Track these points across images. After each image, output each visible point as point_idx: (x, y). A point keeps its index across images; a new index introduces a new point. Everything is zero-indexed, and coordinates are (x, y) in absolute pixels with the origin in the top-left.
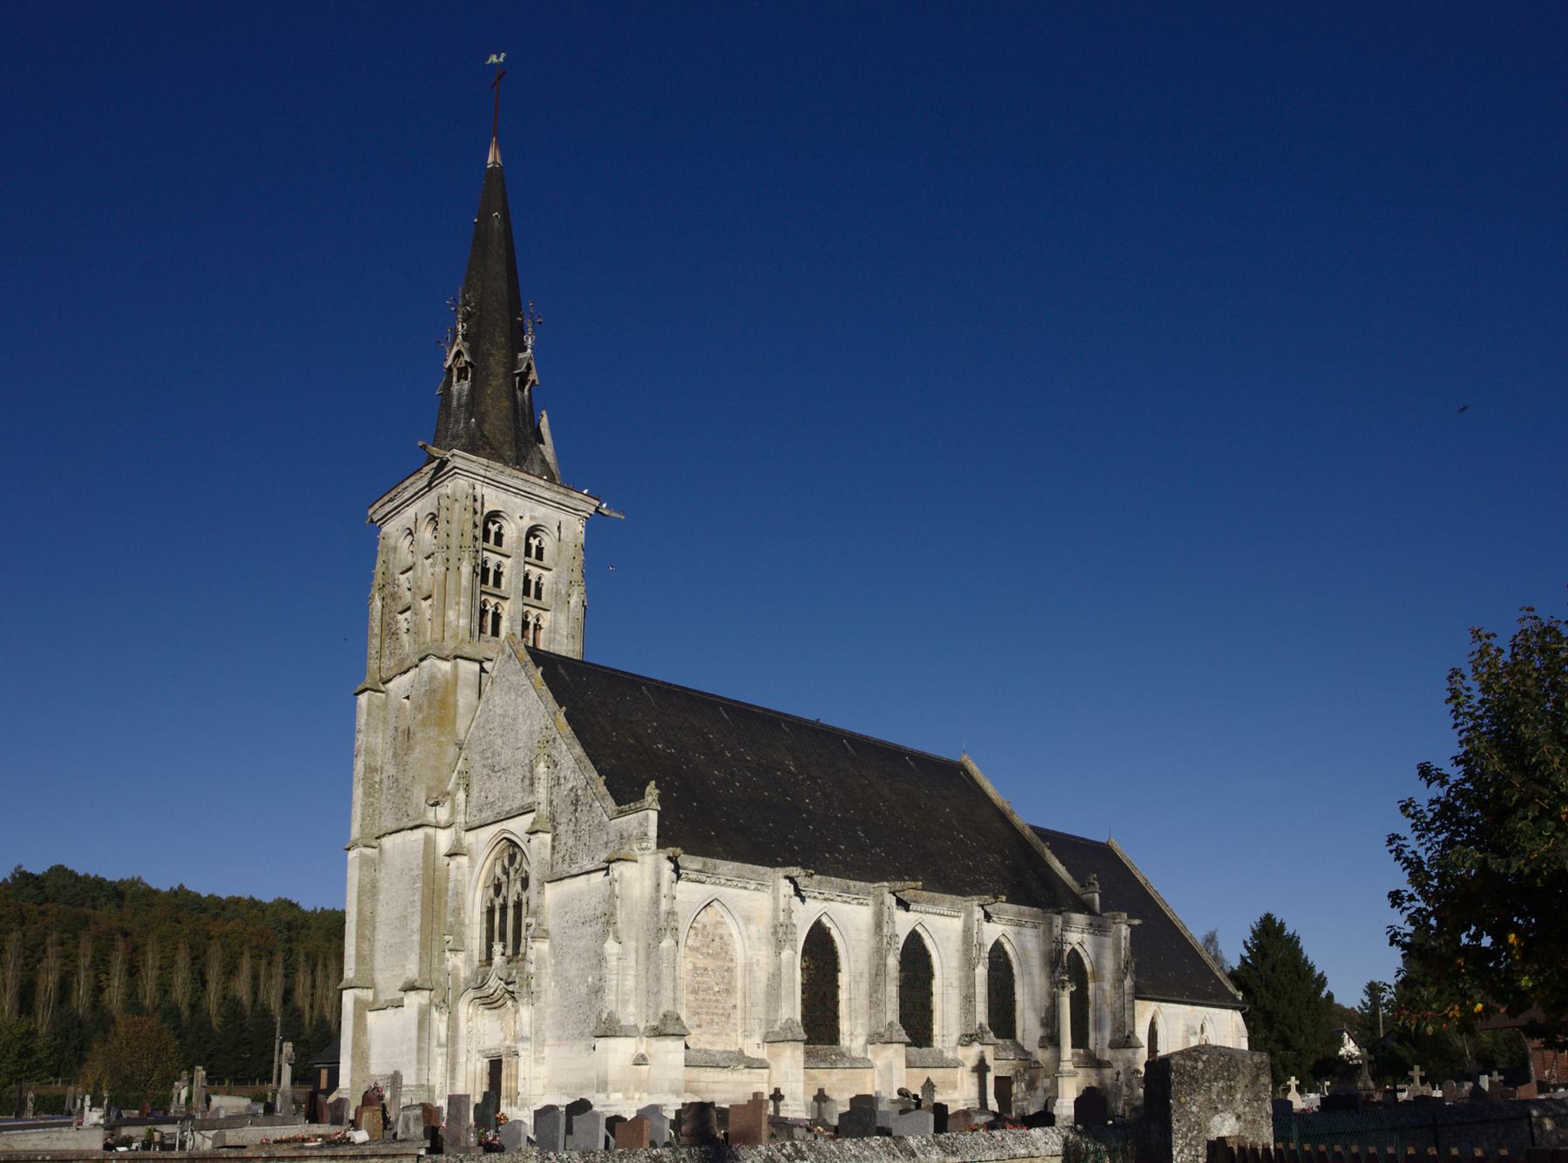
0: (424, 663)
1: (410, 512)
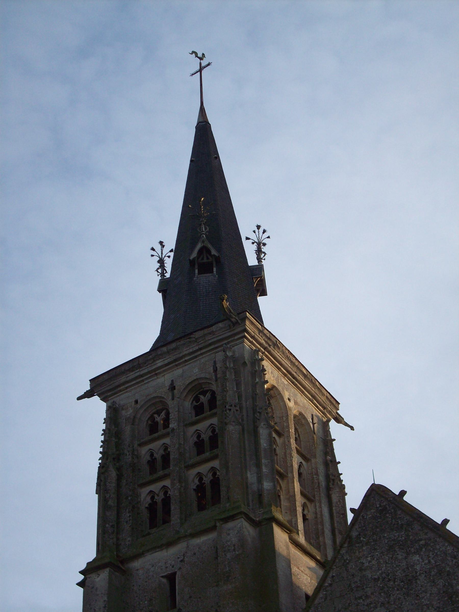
0: (230, 525)
1: (165, 380)
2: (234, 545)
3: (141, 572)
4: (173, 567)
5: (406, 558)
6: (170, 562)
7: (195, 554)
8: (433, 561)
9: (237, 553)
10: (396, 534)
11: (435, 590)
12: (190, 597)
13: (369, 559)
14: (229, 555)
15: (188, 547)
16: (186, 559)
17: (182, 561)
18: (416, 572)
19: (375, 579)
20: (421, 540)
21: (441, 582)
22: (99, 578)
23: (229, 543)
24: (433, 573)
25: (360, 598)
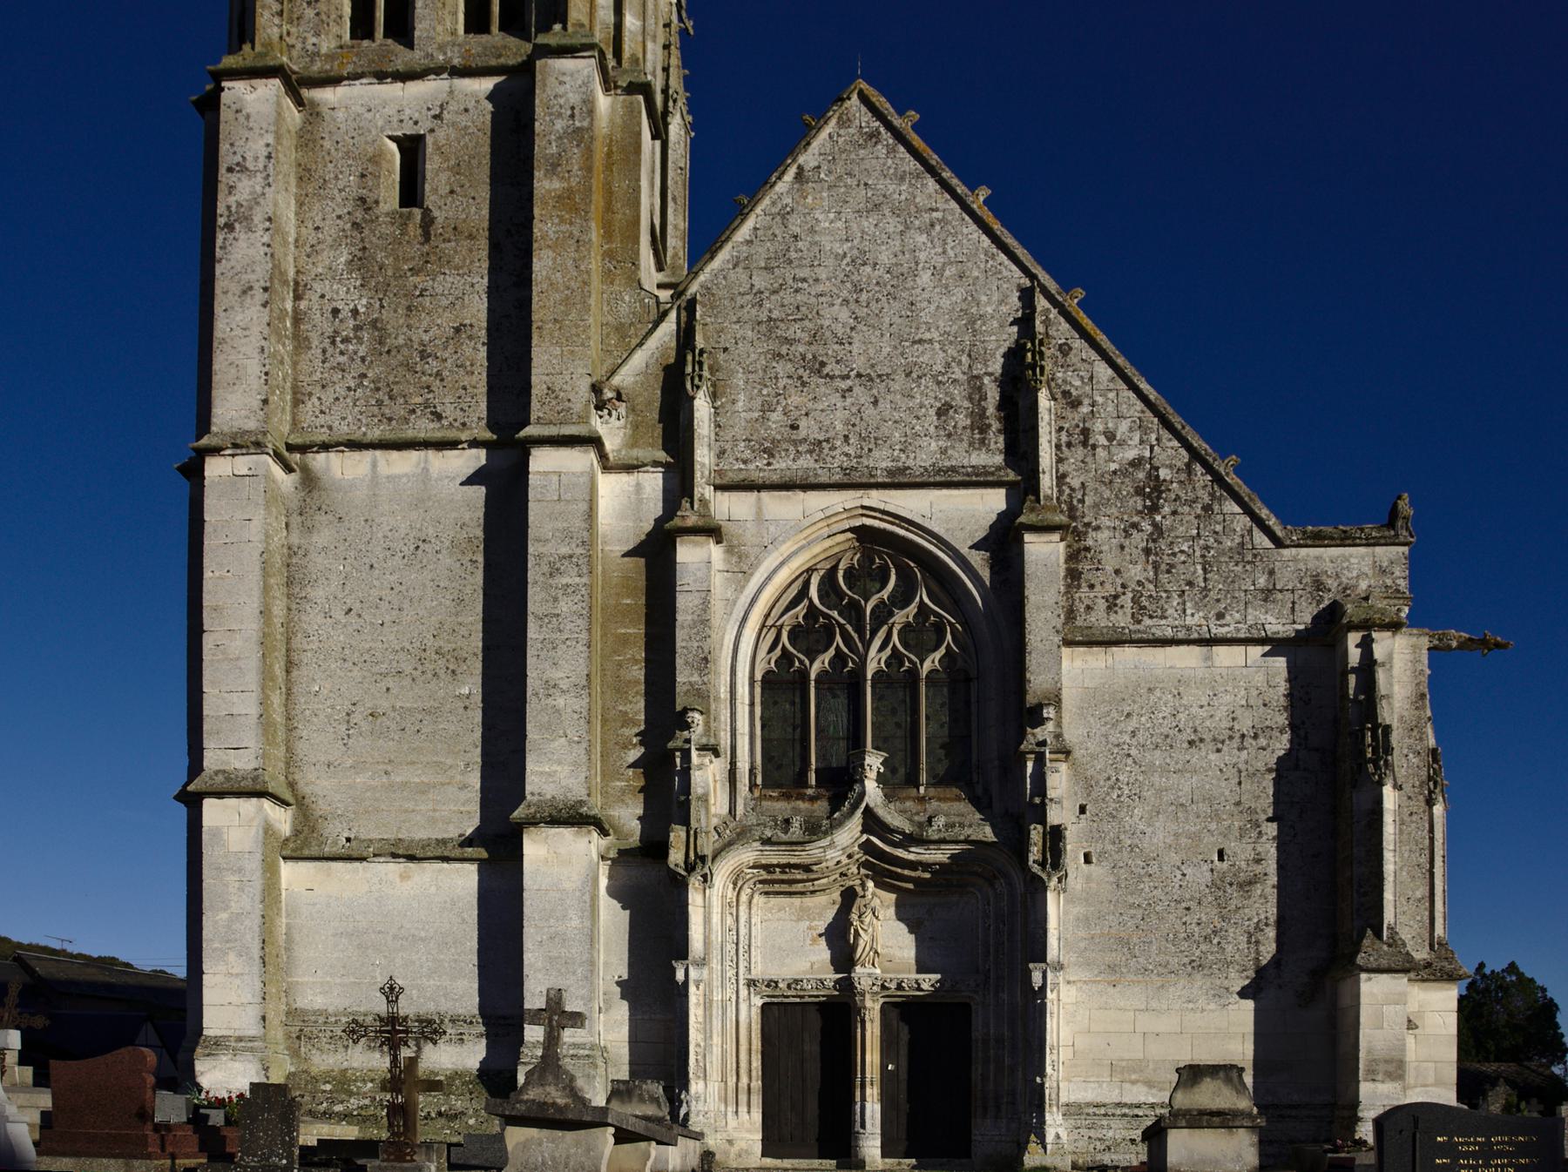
2: (573, 108)
3: (340, 115)
4: (416, 123)
5: (902, 233)
6: (408, 112)
7: (466, 110)
8: (951, 253)
9: (578, 124)
10: (891, 188)
11: (946, 303)
12: (452, 192)
13: (832, 216)
14: (560, 125)
15: (451, 92)
16: (446, 115)
17: (435, 117)
18: (917, 263)
19: (837, 255)
20: (937, 210)
21: (959, 293)
22: (254, 96)
23: (562, 101)
24: (947, 273)
25: (804, 280)
